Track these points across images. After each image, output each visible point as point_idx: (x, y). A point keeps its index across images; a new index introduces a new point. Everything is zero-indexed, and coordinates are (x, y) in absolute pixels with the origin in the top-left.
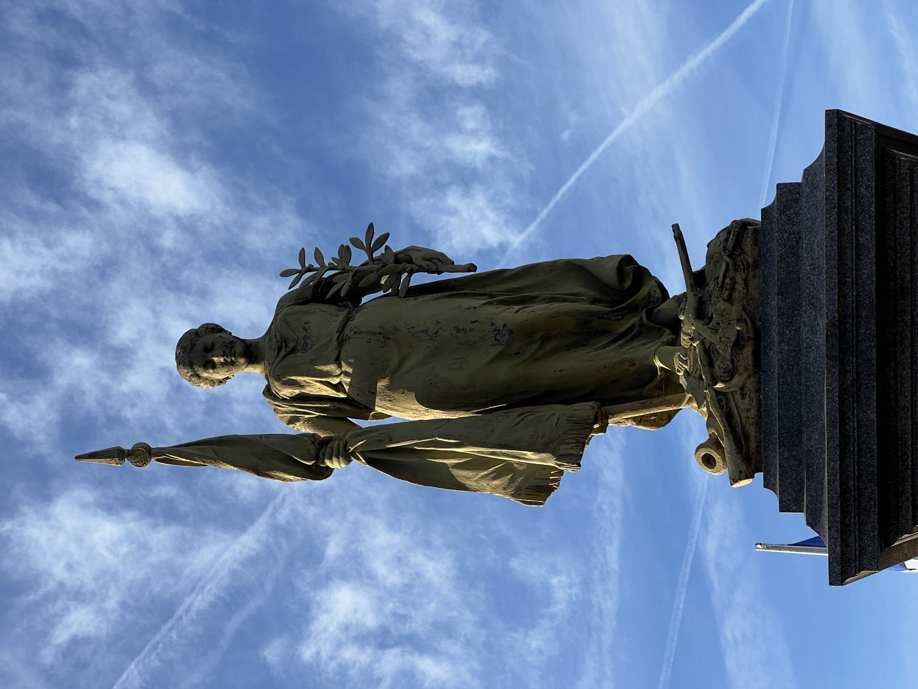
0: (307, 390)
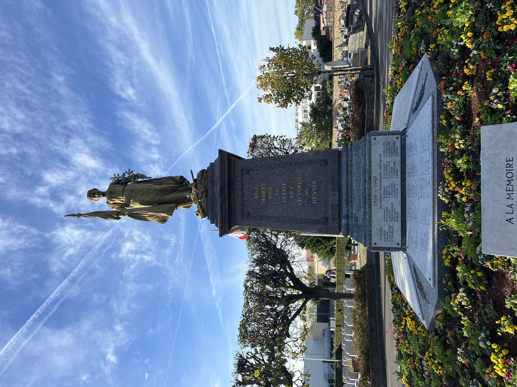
0: (116, 202)
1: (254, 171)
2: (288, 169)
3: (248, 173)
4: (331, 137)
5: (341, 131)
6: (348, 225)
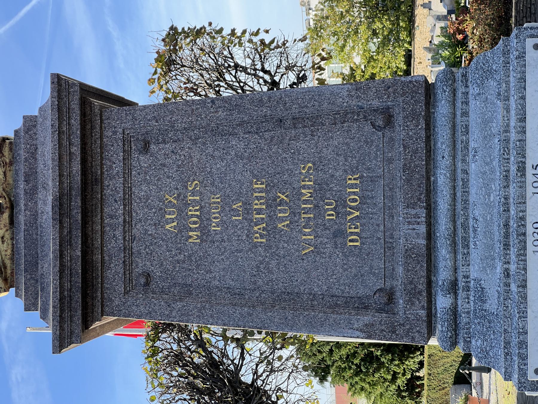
1: (164, 142)
2: (272, 138)
3: (145, 148)
4: (411, 33)
5: (439, 18)
6: (454, 312)
